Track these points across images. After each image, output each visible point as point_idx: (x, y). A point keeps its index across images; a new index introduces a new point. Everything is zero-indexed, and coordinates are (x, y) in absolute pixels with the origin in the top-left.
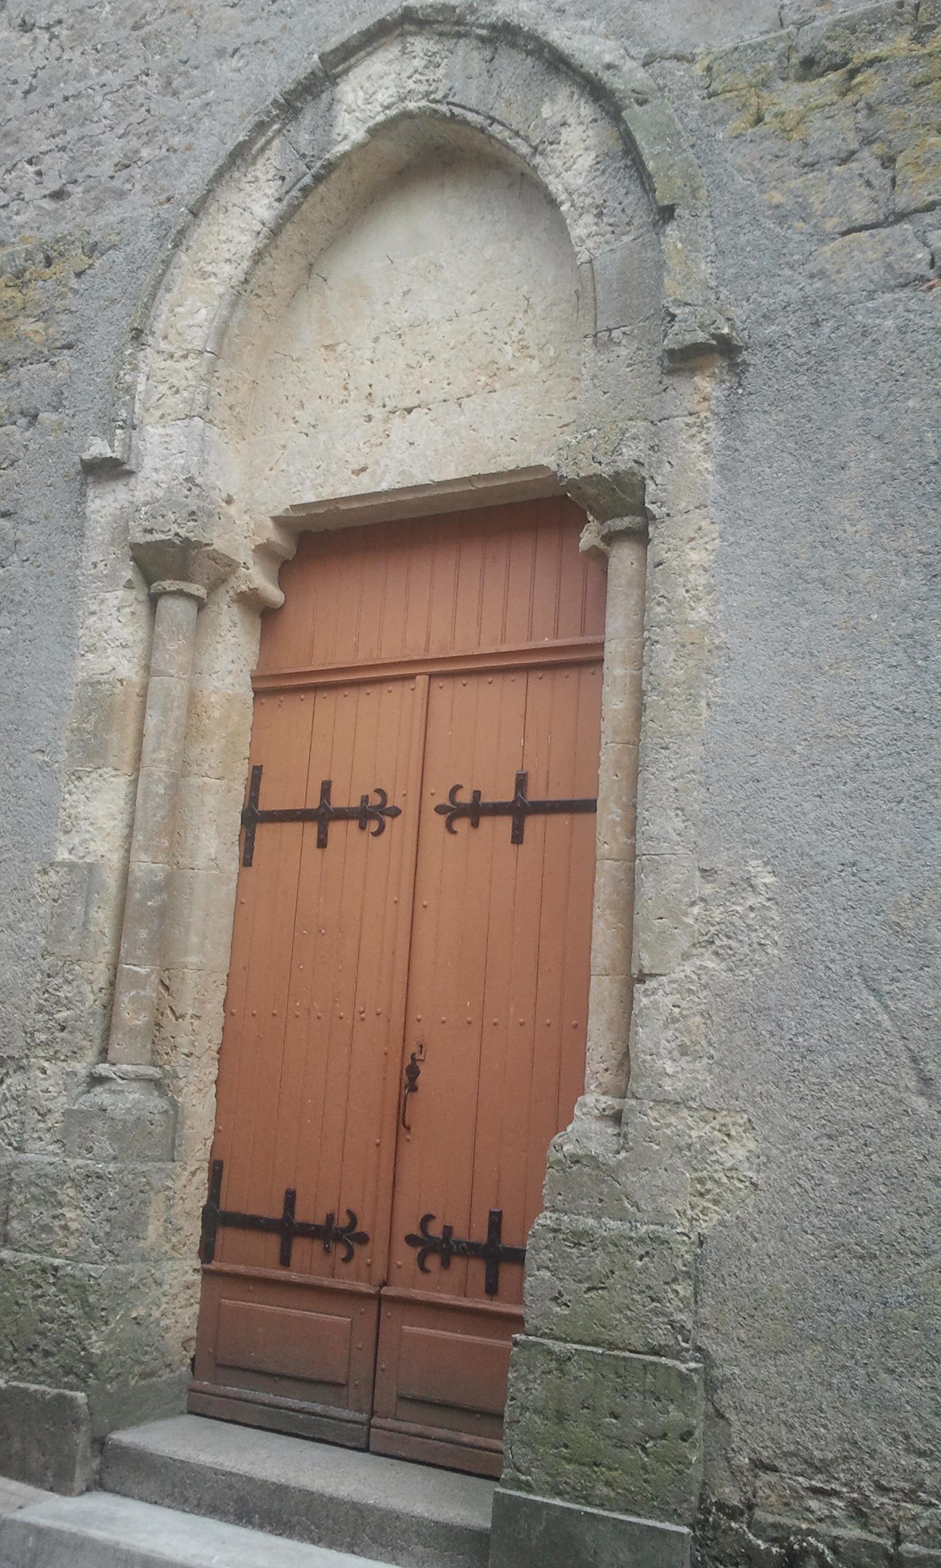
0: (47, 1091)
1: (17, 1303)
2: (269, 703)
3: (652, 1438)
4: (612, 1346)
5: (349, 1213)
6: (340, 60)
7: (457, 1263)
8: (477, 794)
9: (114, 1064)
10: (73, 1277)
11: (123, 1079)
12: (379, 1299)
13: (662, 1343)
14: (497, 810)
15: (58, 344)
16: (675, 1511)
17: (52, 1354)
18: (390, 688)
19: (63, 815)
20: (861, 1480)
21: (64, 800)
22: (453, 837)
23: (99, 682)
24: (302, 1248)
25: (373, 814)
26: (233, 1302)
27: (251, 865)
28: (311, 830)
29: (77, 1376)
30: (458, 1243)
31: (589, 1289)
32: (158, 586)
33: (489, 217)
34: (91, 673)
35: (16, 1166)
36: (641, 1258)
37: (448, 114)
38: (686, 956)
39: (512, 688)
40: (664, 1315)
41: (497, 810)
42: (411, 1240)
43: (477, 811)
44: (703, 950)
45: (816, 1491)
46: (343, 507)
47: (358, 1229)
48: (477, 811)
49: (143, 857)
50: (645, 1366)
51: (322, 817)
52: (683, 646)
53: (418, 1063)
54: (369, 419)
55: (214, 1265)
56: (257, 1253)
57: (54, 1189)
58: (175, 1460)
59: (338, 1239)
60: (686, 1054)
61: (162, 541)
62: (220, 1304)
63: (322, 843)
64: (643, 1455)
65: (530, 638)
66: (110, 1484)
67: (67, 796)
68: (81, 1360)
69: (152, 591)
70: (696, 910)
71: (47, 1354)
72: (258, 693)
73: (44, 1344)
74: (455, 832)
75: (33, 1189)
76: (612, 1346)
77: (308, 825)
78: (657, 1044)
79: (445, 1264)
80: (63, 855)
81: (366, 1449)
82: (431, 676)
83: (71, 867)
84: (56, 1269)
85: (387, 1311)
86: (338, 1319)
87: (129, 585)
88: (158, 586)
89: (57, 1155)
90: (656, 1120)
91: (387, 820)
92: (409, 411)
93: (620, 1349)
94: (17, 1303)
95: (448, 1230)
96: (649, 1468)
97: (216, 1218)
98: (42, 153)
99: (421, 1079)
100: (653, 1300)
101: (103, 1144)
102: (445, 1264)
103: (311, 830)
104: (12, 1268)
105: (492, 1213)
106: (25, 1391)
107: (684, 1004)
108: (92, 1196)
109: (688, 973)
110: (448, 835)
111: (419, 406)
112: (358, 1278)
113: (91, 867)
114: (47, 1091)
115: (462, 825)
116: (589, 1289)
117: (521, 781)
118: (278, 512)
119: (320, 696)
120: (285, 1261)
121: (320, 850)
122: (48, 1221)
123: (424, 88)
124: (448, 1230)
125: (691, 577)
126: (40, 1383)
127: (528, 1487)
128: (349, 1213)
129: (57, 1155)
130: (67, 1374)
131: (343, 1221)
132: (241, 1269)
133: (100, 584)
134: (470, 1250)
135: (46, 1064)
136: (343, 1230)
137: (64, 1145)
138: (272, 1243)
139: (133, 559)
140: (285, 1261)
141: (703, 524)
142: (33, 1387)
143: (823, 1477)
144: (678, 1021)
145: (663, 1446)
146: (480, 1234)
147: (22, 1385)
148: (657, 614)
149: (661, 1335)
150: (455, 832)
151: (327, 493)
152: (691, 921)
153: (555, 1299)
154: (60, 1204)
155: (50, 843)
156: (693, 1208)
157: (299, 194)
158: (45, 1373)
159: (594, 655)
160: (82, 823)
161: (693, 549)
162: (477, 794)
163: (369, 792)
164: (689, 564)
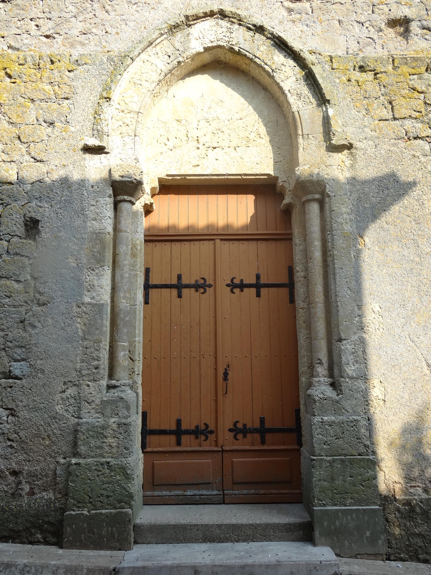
0: (91, 394)
1: (90, 479)
2: (150, 245)
3: (364, 481)
4: (345, 455)
5: (205, 424)
6: (190, 20)
7: (249, 435)
8: (242, 281)
9: (117, 381)
10: (118, 464)
11: (124, 386)
12: (223, 451)
13: (362, 451)
14: (250, 286)
15: (61, 96)
16: (374, 502)
17: (111, 496)
18: (225, 243)
19: (86, 284)
20: (425, 481)
21: (86, 278)
22: (234, 294)
23: (100, 233)
24: (185, 438)
25: (200, 286)
26: (159, 462)
27: (148, 304)
28: (175, 292)
29: (125, 502)
30: (249, 429)
31: (336, 439)
32: (120, 198)
33: (241, 89)
34: (95, 229)
35: (78, 424)
36: (352, 427)
37: (237, 51)
38: (355, 333)
39: (252, 245)
40: (362, 443)
41: (250, 286)
42: (230, 430)
43: (242, 286)
44: (360, 331)
45: (411, 487)
46: (188, 178)
47: (209, 429)
48: (242, 286)
49: (123, 301)
50: (360, 460)
51: (179, 287)
52: (345, 237)
53: (228, 371)
54: (198, 148)
55: (148, 449)
56: (168, 443)
57: (102, 431)
58: (170, 525)
59: (202, 433)
60: (358, 363)
61: (128, 181)
62: (153, 463)
63: (180, 296)
64: (362, 487)
65: (257, 230)
66: (140, 541)
67: (87, 277)
68: (126, 496)
69: (116, 200)
70: (357, 319)
71: (108, 496)
72: (146, 241)
73: (105, 493)
74: (234, 293)
75: (90, 433)
76: (345, 455)
77: (173, 290)
78: (348, 361)
79: (245, 437)
80: (87, 300)
81: (224, 503)
82: (221, 240)
83: (94, 305)
84: (108, 463)
85: (225, 455)
86: (207, 461)
87: (110, 196)
88: (120, 198)
89: (99, 418)
90: (351, 384)
91: (207, 289)
92: (215, 148)
93: (348, 456)
94: (90, 479)
95: (245, 425)
96: (365, 491)
97: (146, 432)
98: (38, 18)
99: (229, 377)
100: (357, 439)
101: (123, 412)
102: (245, 437)
103: (175, 292)
104: (85, 466)
105: (261, 418)
106: (101, 513)
107: (356, 348)
108: (122, 432)
109: (356, 338)
110: (232, 294)
111: (219, 147)
112: (211, 446)
113: (103, 305)
114: (91, 394)
115: (237, 291)
116: (336, 439)
117: (258, 277)
118: (160, 176)
119: (173, 244)
120: (179, 443)
121: (179, 299)
122: (101, 444)
123: (227, 39)
124: (245, 425)
125: (344, 216)
126: (106, 509)
127: (324, 505)
128: (205, 424)
129: (99, 418)
130: (119, 503)
131: (203, 427)
132: (160, 449)
133: (96, 194)
134: (254, 431)
135: (89, 383)
136: (204, 430)
137: (103, 414)
138: (173, 438)
139: (112, 186)
140: (179, 443)
141: (346, 200)
142: (104, 511)
143: (414, 482)
144: (354, 353)
145: (368, 483)
146: (257, 425)
147: (98, 511)
148: (334, 226)
149: (362, 449)
150: (234, 293)
151: (182, 172)
152: (356, 322)
153: (324, 444)
154: (106, 437)
155: (81, 295)
156: (365, 409)
157: (177, 63)
158: (108, 504)
159: (290, 237)
160: (97, 288)
161: (344, 207)
162: (242, 281)
163: (198, 278)
164: (343, 212)
